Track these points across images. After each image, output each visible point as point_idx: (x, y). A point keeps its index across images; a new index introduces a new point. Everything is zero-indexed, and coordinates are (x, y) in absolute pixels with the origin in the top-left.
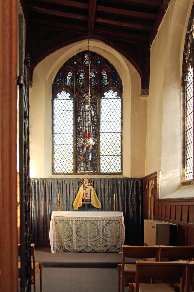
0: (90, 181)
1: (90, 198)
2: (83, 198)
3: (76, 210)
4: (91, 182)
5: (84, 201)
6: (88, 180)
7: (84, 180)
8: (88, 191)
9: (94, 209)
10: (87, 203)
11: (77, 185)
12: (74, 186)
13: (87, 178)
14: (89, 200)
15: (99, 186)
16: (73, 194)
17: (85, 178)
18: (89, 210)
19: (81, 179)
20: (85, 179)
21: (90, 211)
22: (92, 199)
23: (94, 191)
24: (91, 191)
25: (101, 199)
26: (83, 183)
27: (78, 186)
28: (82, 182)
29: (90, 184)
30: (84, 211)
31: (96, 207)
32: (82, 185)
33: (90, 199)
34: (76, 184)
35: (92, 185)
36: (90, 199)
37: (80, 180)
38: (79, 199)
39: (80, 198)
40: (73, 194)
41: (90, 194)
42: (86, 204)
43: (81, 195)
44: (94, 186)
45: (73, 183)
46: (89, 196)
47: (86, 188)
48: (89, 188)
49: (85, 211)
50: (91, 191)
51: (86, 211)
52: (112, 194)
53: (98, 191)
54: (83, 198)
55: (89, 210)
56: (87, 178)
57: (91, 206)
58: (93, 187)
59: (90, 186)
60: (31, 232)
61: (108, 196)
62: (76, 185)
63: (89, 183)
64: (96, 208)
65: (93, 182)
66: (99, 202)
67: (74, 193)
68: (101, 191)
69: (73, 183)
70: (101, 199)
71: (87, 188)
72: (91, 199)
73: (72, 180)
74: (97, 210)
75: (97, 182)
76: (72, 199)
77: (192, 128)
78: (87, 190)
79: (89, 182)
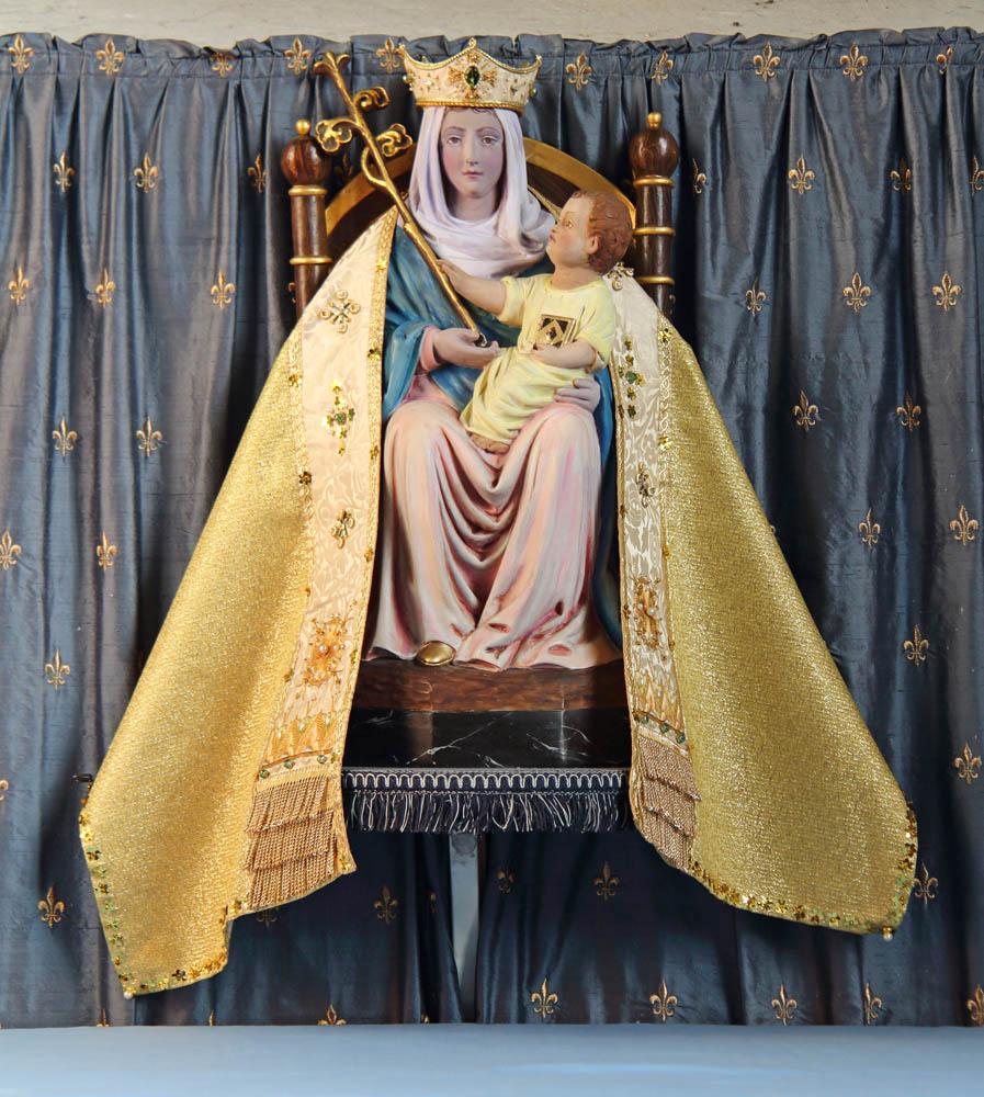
0: (571, 144)
1: (602, 624)
2: (390, 637)
3: (155, 1008)
4: (619, 170)
5: (422, 718)
6: (510, 86)
7: (404, 109)
8: (534, 412)
9: (708, 970)
10: (496, 775)
11: (195, 236)
12: (104, 290)
13: (510, 53)
14: (563, 706)
15: (862, 293)
16: (87, 523)
17: (439, 50)
18: (544, 995)
19: (316, 78)
20: (432, 84)
21: (570, 1014)
22: (643, 668)
23: (694, 434)
24: (606, 418)
25: (913, 646)
26: (376, 204)
27: (223, 291)
28: (337, 170)
29: (578, 208)
30: (394, 1015)
31: (745, 890)
32: (339, 243)
33: (580, 658)
34: (168, 219)
35: (636, 261)
36: (580, 658)
37: (287, 98)
38: (268, 681)
39: (293, 639)
40: (87, 523)
41: (527, 448)
42: (486, 805)
43: (319, 532)
44: (711, 285)
45: (67, 207)
46: (570, 586)
47: (453, 341)
48: (557, 327)
49: (434, 1013)
50: (606, 418)
51: (471, 1015)
52: (886, 573)
53: (808, 413)
54: (390, 637)
55: (544, 995)
56: (510, 53)
57: (606, 878)
58: (685, 313)
59: (600, 262)
60: (689, 562)
61: (49, 601)
62: (168, 252)
63: (549, 187)
64: (773, 931)
65: (686, 159)
66: (860, 743)
67: (117, 475)
68: (921, 435)
69: (67, 207)
70: (913, 646)
71: (500, 334)
72: (609, 678)
73: (66, 104)
74: (785, 1000)
75: (800, 176)
76: (62, 668)
77: (285, 827)
78: (490, 412)
79: (557, 162)
